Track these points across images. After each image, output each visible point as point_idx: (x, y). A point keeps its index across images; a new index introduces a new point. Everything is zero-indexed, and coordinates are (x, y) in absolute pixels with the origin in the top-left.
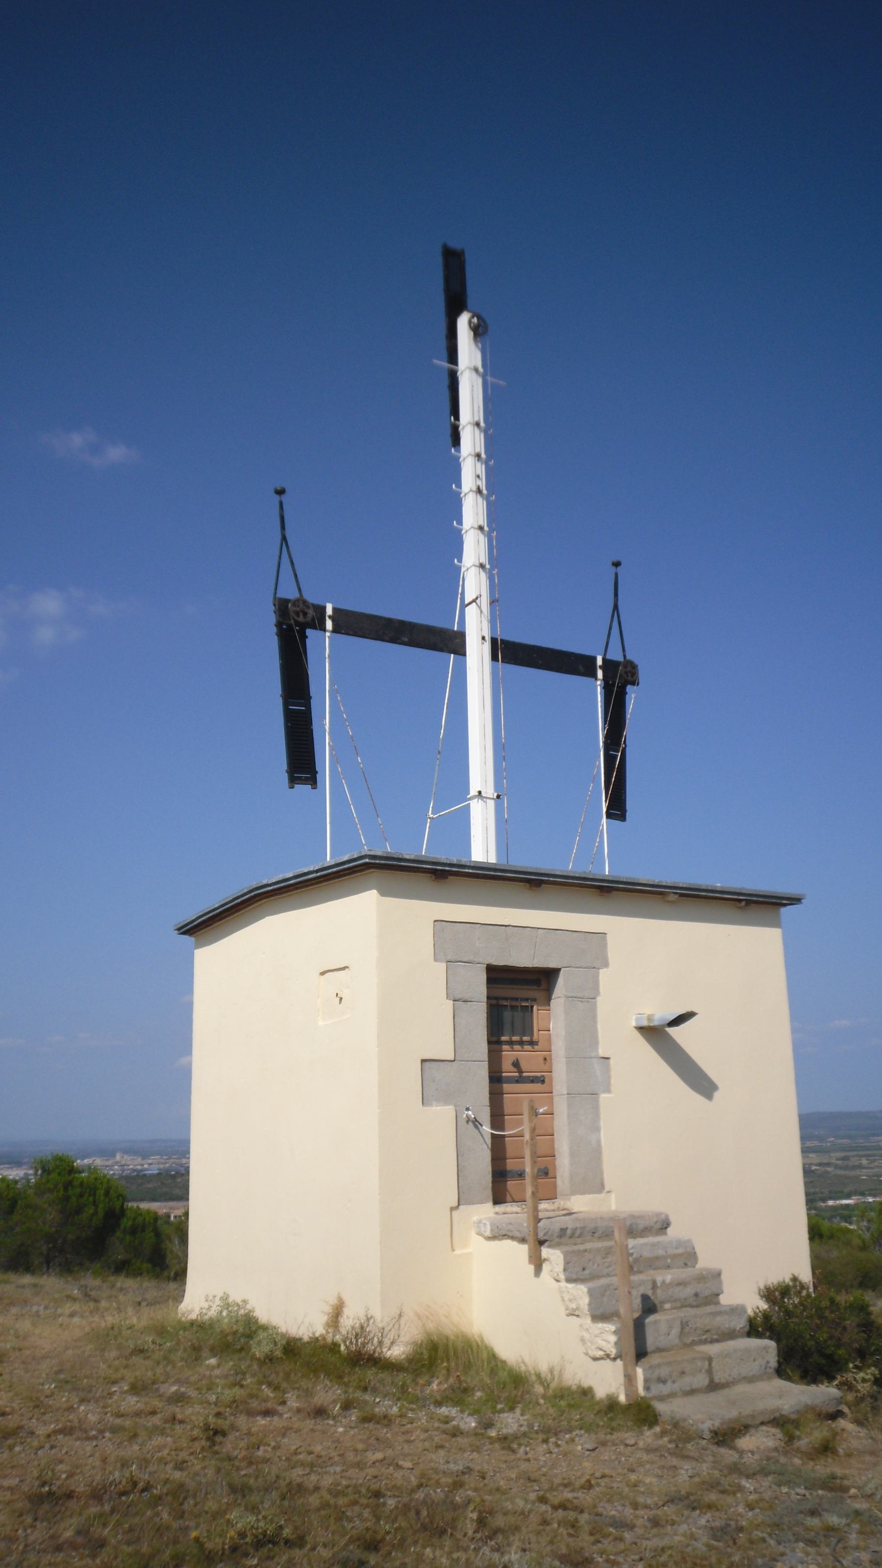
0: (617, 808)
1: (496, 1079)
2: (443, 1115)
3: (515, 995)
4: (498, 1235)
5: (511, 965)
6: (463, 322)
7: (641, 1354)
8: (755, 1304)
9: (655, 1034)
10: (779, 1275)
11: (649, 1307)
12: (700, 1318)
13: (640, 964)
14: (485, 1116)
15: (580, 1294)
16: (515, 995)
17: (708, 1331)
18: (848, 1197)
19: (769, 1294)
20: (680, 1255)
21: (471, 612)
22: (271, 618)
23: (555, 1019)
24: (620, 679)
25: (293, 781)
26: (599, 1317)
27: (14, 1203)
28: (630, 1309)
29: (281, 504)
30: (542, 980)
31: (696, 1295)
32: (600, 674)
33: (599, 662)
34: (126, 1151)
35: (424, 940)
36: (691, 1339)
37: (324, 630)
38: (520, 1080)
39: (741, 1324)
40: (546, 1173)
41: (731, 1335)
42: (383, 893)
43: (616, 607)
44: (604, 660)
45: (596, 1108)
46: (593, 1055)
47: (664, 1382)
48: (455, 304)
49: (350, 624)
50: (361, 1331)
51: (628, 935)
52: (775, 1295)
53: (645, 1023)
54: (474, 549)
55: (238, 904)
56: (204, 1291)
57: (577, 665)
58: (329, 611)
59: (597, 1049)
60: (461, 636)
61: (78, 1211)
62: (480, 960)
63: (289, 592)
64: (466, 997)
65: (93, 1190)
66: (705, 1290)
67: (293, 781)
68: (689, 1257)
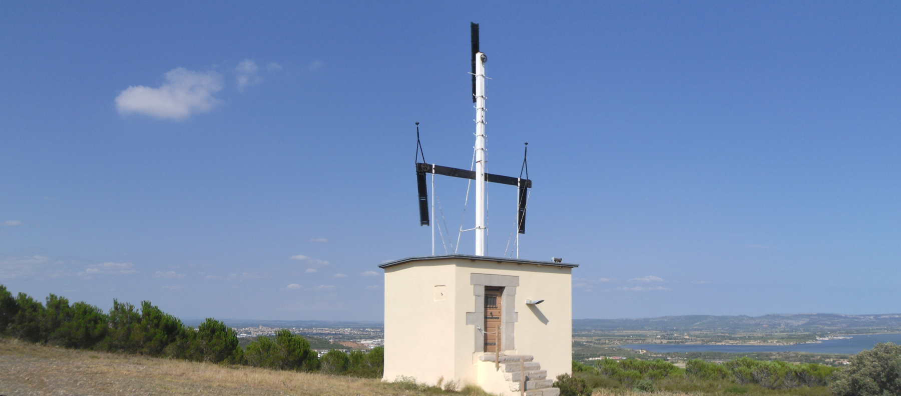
0: (522, 229)
1: (486, 318)
2: (472, 328)
3: (492, 293)
4: (486, 360)
6: (478, 56)
7: (525, 390)
8: (555, 380)
9: (532, 306)
10: (562, 372)
11: (527, 379)
12: (541, 382)
13: (528, 285)
14: (483, 328)
15: (510, 375)
16: (492, 293)
18: (599, 356)
19: (559, 378)
21: (478, 165)
23: (503, 301)
24: (525, 185)
25: (422, 224)
26: (515, 381)
27: (270, 347)
28: (523, 379)
30: (500, 289)
34: (264, 325)
35: (468, 279)
38: (492, 318)
39: (551, 384)
40: (499, 345)
41: (548, 387)
42: (457, 265)
48: (475, 49)
49: (440, 170)
50: (449, 385)
51: (525, 277)
52: (561, 378)
54: (479, 143)
56: (391, 373)
57: (511, 181)
60: (474, 173)
61: (294, 350)
65: (299, 344)
66: (542, 376)
67: (422, 224)
68: (539, 367)
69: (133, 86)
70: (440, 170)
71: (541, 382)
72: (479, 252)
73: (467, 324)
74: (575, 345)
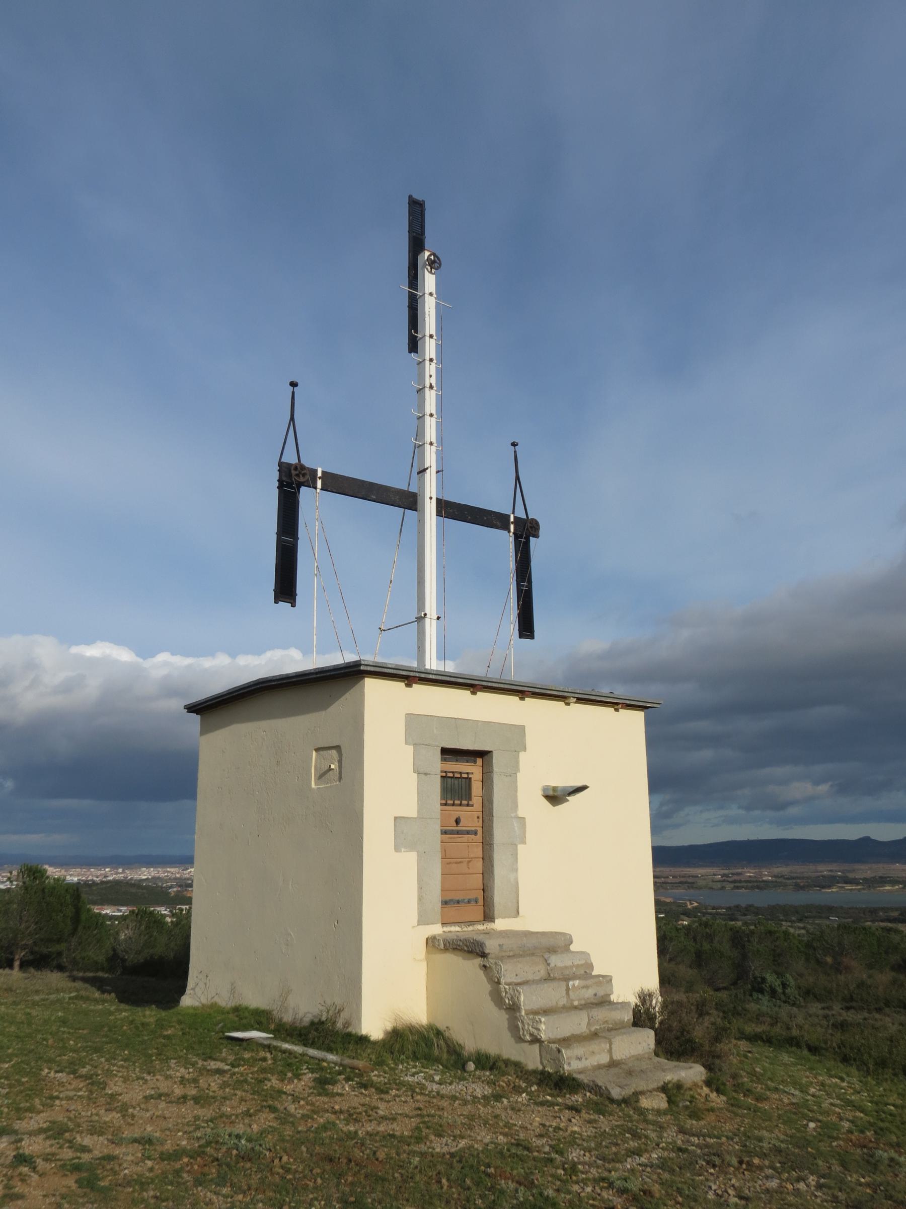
2: (410, 859)
5: (217, 732)
20: (582, 965)
22: (274, 476)
24: (526, 530)
29: (293, 393)
31: (595, 995)
32: (512, 527)
33: (512, 519)
37: (316, 488)
41: (617, 1028)
43: (518, 478)
44: (515, 517)
45: (515, 855)
46: (513, 815)
49: (336, 484)
53: (551, 793)
55: (243, 693)
58: (320, 474)
60: (439, 514)
63: (290, 458)
64: (427, 771)
69: (519, 614)
70: (336, 484)
71: (600, 1014)
72: (432, 663)
73: (397, 849)
74: (659, 905)
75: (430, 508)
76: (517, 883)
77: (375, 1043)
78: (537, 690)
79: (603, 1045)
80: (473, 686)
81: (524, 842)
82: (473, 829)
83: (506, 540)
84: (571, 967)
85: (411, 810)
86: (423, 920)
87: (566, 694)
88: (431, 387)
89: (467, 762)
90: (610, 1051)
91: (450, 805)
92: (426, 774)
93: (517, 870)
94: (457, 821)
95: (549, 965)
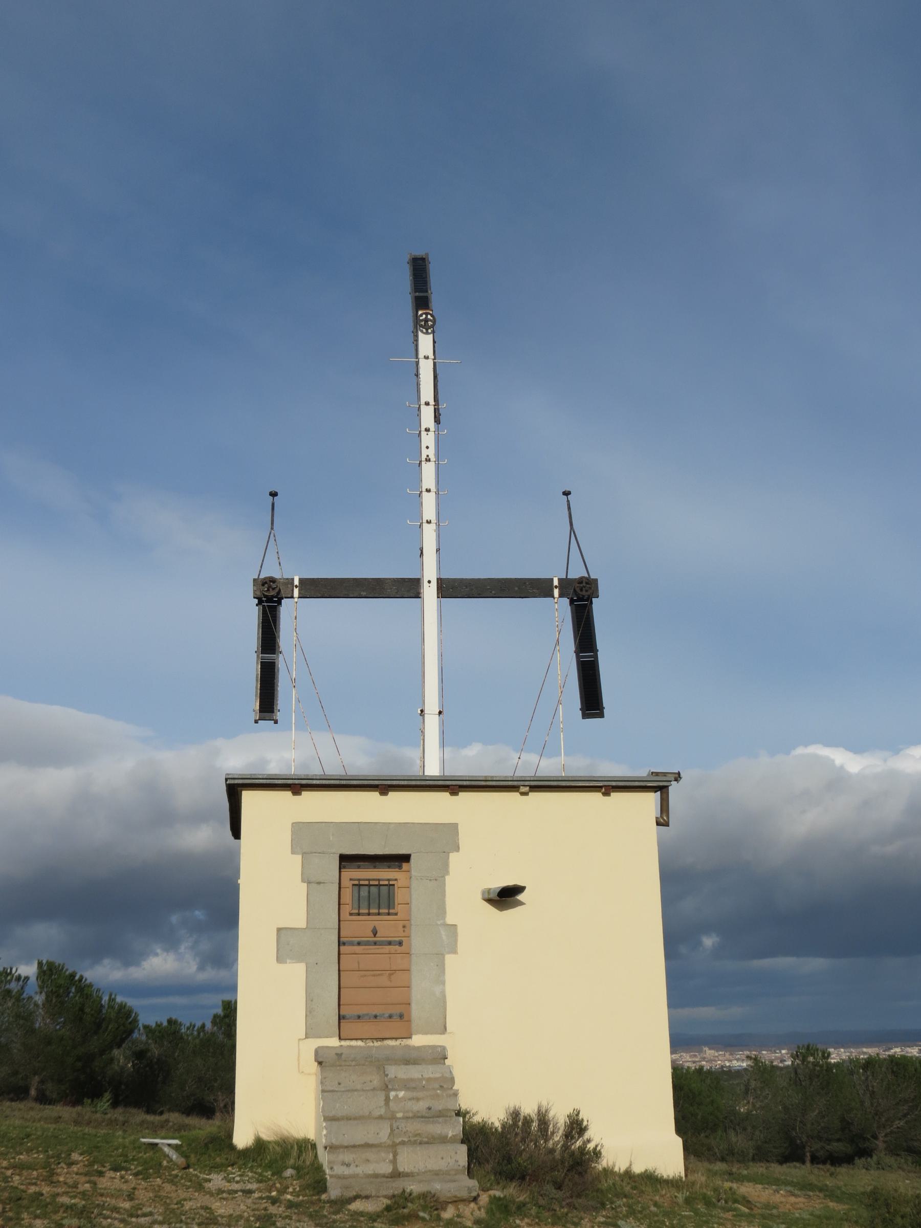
2: (297, 971)
17: (419, 1134)
20: (436, 1079)
24: (581, 595)
31: (429, 1109)
36: (400, 1139)
45: (441, 967)
47: (348, 1165)
49: (316, 588)
59: (444, 917)
62: (334, 851)
73: (280, 959)
75: (430, 592)
76: (444, 996)
77: (232, 1147)
78: (465, 783)
79: (383, 1155)
80: (384, 787)
81: (454, 951)
82: (397, 939)
83: (559, 609)
84: (420, 1080)
85: (299, 920)
86: (309, 1034)
87: (515, 783)
88: (428, 460)
89: (389, 867)
90: (394, 1162)
91: (363, 914)
92: (319, 883)
93: (443, 983)
94: (375, 933)
95: (387, 1075)
